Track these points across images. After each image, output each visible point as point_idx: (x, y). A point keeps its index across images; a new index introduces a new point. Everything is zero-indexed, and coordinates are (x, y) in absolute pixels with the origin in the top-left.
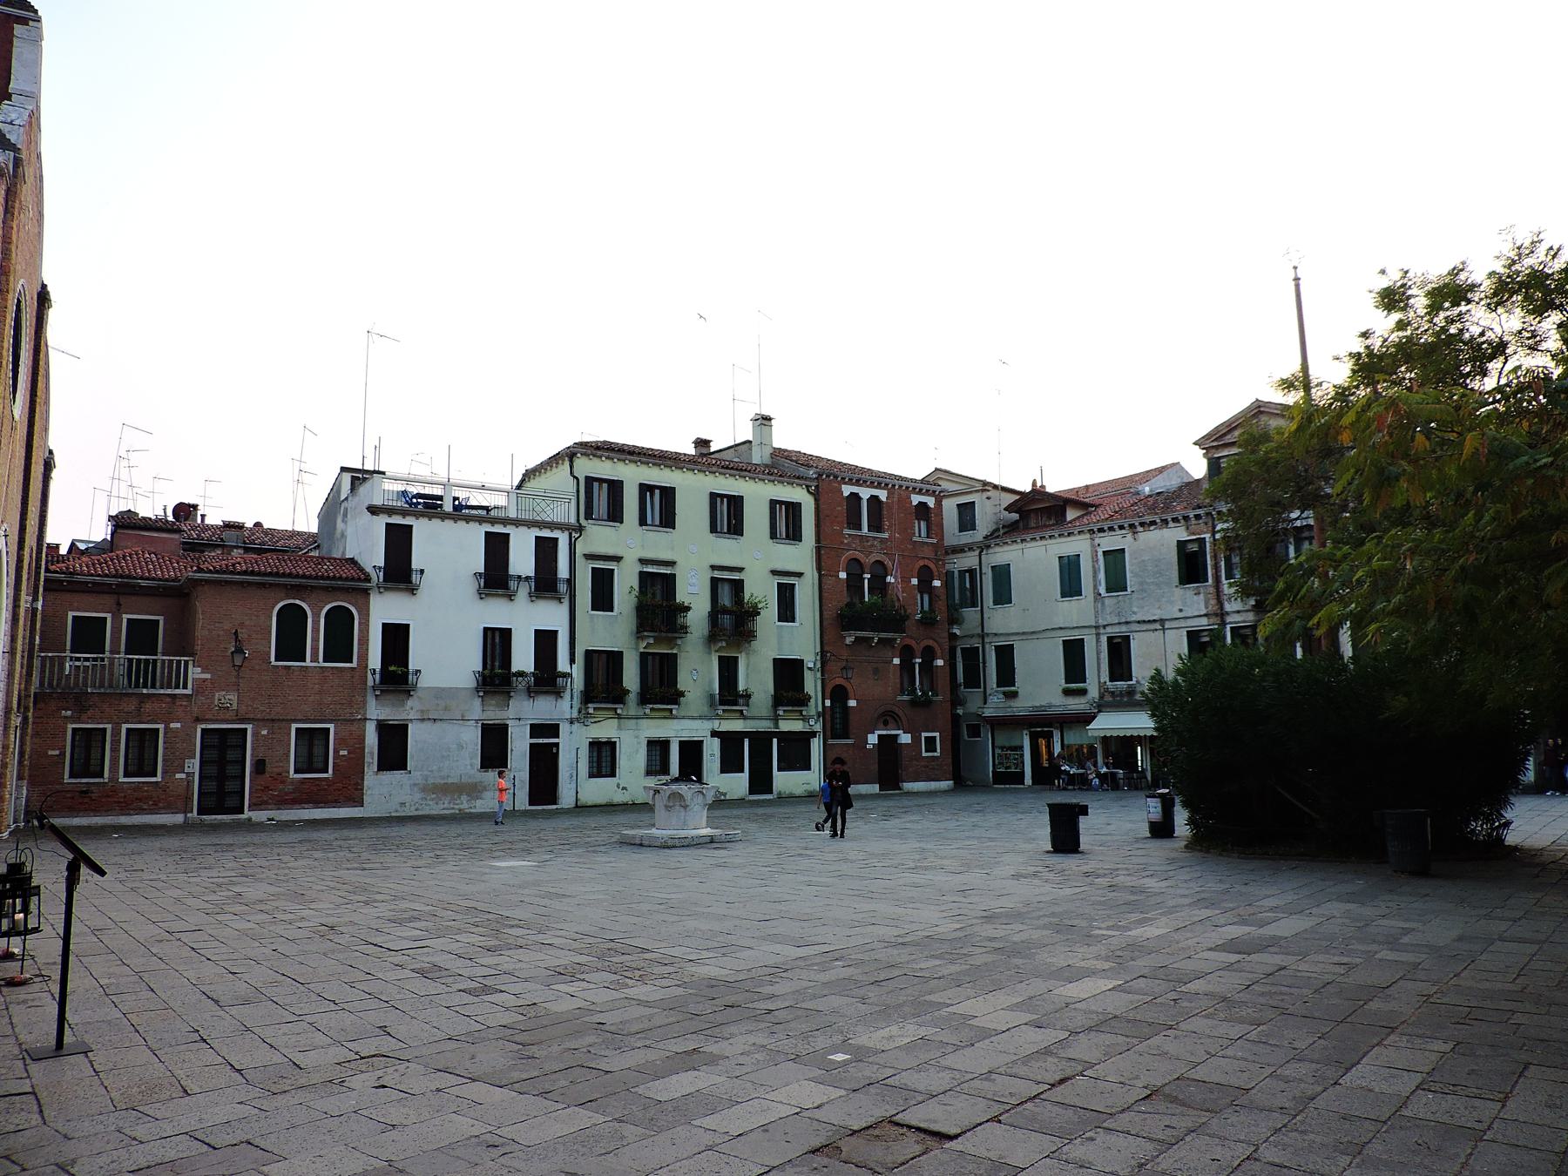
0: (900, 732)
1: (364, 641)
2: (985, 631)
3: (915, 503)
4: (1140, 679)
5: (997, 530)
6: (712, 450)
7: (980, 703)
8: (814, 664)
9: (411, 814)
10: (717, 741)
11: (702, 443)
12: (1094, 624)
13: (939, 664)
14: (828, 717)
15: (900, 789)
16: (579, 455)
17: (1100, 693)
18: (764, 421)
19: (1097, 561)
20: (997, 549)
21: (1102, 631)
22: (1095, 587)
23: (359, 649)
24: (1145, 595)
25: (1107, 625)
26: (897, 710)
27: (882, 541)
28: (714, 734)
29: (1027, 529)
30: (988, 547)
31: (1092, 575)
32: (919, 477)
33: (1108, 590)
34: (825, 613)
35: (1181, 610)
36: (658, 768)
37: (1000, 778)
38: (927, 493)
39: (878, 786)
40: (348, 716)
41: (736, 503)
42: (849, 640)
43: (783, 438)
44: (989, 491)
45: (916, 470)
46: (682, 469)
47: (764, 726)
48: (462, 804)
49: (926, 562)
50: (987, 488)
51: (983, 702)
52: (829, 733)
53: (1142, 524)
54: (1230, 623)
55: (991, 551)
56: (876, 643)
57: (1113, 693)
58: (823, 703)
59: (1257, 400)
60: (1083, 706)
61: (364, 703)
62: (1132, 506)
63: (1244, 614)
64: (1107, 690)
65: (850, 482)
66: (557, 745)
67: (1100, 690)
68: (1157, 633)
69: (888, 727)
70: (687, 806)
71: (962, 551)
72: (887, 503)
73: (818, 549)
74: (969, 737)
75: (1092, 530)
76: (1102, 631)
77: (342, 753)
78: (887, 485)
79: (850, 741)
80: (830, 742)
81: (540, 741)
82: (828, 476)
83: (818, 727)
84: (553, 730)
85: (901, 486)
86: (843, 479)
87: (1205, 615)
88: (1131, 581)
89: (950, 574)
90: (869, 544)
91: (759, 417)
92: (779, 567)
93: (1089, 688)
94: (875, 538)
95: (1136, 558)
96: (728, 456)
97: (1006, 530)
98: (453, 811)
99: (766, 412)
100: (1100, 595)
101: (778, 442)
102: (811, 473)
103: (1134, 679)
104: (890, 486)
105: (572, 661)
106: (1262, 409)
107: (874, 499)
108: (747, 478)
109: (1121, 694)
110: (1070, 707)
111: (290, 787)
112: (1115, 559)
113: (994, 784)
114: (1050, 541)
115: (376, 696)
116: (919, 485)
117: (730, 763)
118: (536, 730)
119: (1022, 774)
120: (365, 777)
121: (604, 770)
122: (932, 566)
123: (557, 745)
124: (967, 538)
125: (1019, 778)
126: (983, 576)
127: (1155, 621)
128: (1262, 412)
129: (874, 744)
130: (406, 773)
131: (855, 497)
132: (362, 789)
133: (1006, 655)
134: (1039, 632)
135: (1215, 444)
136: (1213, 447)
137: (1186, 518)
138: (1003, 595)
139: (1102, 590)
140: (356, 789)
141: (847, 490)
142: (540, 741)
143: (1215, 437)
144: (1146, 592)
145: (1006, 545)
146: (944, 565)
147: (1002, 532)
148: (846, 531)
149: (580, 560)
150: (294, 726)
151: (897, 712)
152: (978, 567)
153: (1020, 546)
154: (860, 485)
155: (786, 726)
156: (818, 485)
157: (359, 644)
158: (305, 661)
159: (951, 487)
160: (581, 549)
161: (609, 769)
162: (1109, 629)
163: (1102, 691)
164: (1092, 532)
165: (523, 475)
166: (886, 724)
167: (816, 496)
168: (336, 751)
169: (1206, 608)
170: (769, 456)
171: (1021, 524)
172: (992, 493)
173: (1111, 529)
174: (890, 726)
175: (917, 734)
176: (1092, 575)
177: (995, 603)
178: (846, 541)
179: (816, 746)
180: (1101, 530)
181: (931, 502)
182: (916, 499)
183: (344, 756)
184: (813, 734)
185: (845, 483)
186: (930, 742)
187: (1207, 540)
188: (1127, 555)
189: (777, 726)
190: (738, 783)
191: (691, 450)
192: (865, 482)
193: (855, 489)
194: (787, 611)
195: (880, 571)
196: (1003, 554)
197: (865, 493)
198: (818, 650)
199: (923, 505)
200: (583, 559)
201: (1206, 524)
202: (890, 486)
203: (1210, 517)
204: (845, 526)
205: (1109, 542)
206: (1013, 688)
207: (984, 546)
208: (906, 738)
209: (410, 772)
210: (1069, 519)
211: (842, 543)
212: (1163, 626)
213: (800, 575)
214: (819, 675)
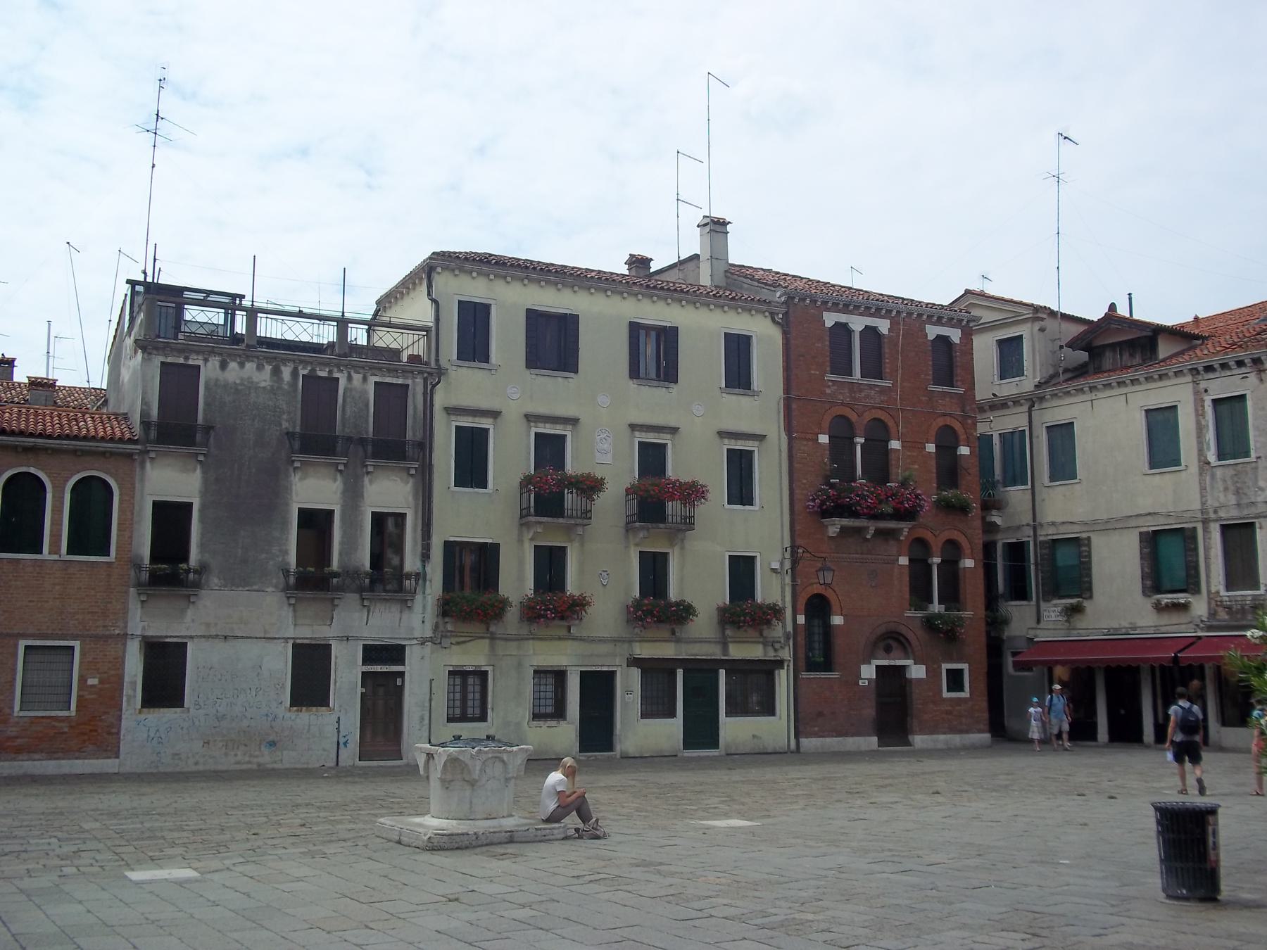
0: (909, 662)
1: (128, 525)
2: (1038, 520)
3: (931, 337)
5: (1055, 375)
6: (652, 270)
9: (189, 770)
10: (636, 673)
11: (638, 263)
14: (801, 639)
16: (439, 270)
17: (1209, 609)
18: (716, 227)
19: (1203, 415)
20: (1055, 402)
22: (1201, 452)
23: (118, 536)
26: (903, 630)
27: (883, 390)
28: (634, 662)
29: (1099, 371)
30: (1042, 399)
32: (946, 302)
33: (1221, 456)
34: (797, 491)
36: (550, 710)
38: (951, 323)
39: (875, 739)
40: (100, 631)
41: (667, 337)
42: (833, 531)
43: (740, 253)
44: (1042, 319)
45: (943, 295)
46: (589, 289)
47: (713, 652)
48: (263, 756)
49: (949, 421)
50: (1040, 315)
52: (802, 663)
57: (1229, 608)
58: (794, 620)
60: (1184, 626)
61: (125, 611)
62: (1258, 334)
64: (1220, 604)
65: (835, 307)
66: (402, 674)
69: (892, 654)
70: (476, 781)
71: (1004, 405)
72: (889, 337)
75: (1196, 369)
77: (91, 682)
79: (835, 675)
80: (804, 675)
81: (378, 668)
83: (786, 654)
84: (394, 653)
88: (1256, 441)
89: (986, 440)
90: (863, 394)
91: (708, 220)
94: (871, 387)
96: (673, 276)
97: (1069, 375)
98: (249, 766)
99: (717, 214)
100: (1209, 463)
101: (736, 256)
102: (778, 296)
104: (894, 313)
105: (425, 557)
107: (870, 332)
108: (684, 303)
110: (1163, 629)
111: (14, 729)
115: (143, 602)
116: (946, 314)
117: (656, 706)
118: (373, 653)
120: (123, 716)
121: (470, 711)
122: (957, 426)
123: (402, 674)
124: (1009, 388)
130: (183, 712)
131: (842, 330)
132: (118, 733)
138: (1063, 467)
139: (1212, 457)
140: (109, 733)
141: (830, 319)
142: (378, 668)
146: (974, 425)
147: (1062, 378)
148: (830, 377)
149: (439, 418)
150: (22, 644)
152: (1027, 429)
154: (851, 313)
155: (738, 652)
156: (787, 312)
157: (119, 530)
158: (41, 553)
159: (987, 317)
160: (440, 399)
161: (477, 711)
163: (1213, 603)
164: (1195, 371)
165: (378, 303)
166: (888, 650)
167: (786, 327)
168: (83, 680)
170: (722, 274)
171: (1091, 368)
172: (1049, 323)
173: (1224, 366)
175: (935, 666)
177: (1052, 478)
178: (828, 391)
179: (783, 680)
180: (1209, 369)
181: (955, 335)
182: (932, 331)
183: (92, 686)
184: (780, 664)
185: (828, 310)
186: (955, 680)
188: (1249, 403)
189: (725, 650)
190: (669, 731)
191: (624, 270)
192: (857, 307)
193: (843, 318)
194: (741, 491)
195: (878, 435)
196: (1058, 412)
198: (787, 543)
199: (943, 340)
200: (444, 415)
202: (894, 313)
204: (828, 369)
205: (1221, 386)
207: (1033, 401)
208: (917, 672)
209: (188, 709)
210: (1161, 356)
211: (824, 393)
213: (761, 438)
214: (788, 579)
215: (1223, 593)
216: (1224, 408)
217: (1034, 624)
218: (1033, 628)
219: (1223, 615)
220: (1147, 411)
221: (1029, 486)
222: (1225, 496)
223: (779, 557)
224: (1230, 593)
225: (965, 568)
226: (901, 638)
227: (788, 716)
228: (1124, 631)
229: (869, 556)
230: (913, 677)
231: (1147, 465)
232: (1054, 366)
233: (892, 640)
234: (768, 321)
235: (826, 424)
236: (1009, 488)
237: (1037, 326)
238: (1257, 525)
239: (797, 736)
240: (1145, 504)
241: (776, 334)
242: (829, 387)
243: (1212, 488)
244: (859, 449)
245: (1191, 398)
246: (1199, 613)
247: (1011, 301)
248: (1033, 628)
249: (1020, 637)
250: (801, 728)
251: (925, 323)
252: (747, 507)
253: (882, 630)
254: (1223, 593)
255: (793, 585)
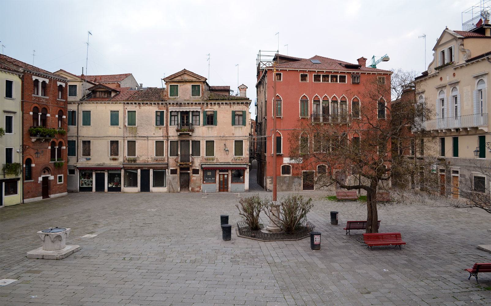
0: (50, 175)
2: (79, 135)
4: (138, 156)
5: (84, 96)
7: (75, 162)
8: (20, 150)
12: (123, 136)
13: (64, 148)
15: (49, 197)
17: (124, 160)
19: (125, 114)
20: (86, 105)
21: (126, 138)
22: (124, 123)
24: (142, 128)
25: (128, 137)
27: (46, 99)
30: (82, 103)
31: (123, 119)
33: (129, 124)
34: (24, 129)
35: (154, 134)
37: (82, 189)
39: (42, 197)
51: (76, 161)
52: (24, 178)
53: (143, 104)
54: (170, 140)
55: (83, 105)
56: (44, 141)
59: (185, 69)
63: (175, 137)
65: (36, 75)
67: (123, 159)
68: (145, 141)
73: (22, 102)
74: (69, 174)
76: (126, 138)
78: (49, 77)
79: (33, 181)
80: (25, 181)
82: (27, 72)
83: (20, 176)
85: (54, 78)
86: (33, 73)
87: (162, 136)
92: (7, 109)
93: (120, 158)
95: (140, 115)
100: (126, 126)
102: (21, 70)
103: (136, 156)
104: (50, 78)
106: (186, 73)
107: (44, 82)
109: (131, 161)
110: (112, 165)
112: (132, 114)
113: (80, 191)
114: (107, 105)
119: (92, 188)
125: (90, 189)
126: (79, 114)
127: (145, 137)
128: (185, 73)
129: (41, 181)
131: (37, 81)
133: (87, 144)
134: (101, 137)
135: (170, 81)
136: (169, 82)
137: (158, 104)
139: (127, 124)
141: (34, 78)
143: (170, 79)
144: (142, 127)
145: (93, 104)
151: (49, 168)
153: (95, 105)
154: (39, 76)
155: (8, 177)
162: (128, 138)
167: (22, 79)
169: (163, 134)
174: (46, 173)
176: (123, 119)
177: (84, 125)
179: (20, 184)
182: (59, 83)
184: (19, 179)
185: (34, 75)
186: (60, 178)
187: (165, 112)
188: (136, 113)
189: (4, 178)
196: (87, 107)
197: (41, 80)
199: (61, 86)
201: (165, 106)
203: (166, 104)
205: (130, 108)
206: (89, 157)
208: (52, 178)
212: (148, 139)
213: (15, 113)
214: (21, 154)
215: (127, 157)
216: (130, 113)
217: (76, 162)
218: (75, 163)
219: (126, 162)
220: (111, 111)
221: (77, 126)
222: (129, 134)
223: (19, 148)
224: (129, 157)
225: (63, 149)
226: (48, 169)
227: (21, 194)
228: (101, 165)
229: (42, 147)
230: (51, 179)
231: (110, 124)
232: (84, 94)
233: (46, 170)
234: (18, 77)
235: (32, 109)
236: (70, 126)
237: (81, 83)
238: (136, 141)
239: (23, 199)
240: (109, 134)
241: (20, 81)
242: (33, 98)
243: (126, 131)
244: (39, 116)
245: (123, 110)
246: (121, 161)
247: (72, 74)
248: (75, 163)
249: (72, 165)
250: (24, 197)
251: (57, 81)
252: (11, 133)
253: (44, 167)
254: (127, 157)
255: (22, 156)
